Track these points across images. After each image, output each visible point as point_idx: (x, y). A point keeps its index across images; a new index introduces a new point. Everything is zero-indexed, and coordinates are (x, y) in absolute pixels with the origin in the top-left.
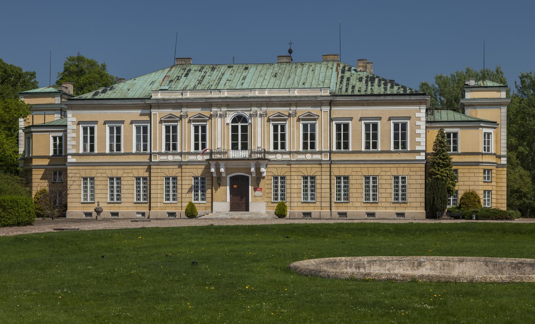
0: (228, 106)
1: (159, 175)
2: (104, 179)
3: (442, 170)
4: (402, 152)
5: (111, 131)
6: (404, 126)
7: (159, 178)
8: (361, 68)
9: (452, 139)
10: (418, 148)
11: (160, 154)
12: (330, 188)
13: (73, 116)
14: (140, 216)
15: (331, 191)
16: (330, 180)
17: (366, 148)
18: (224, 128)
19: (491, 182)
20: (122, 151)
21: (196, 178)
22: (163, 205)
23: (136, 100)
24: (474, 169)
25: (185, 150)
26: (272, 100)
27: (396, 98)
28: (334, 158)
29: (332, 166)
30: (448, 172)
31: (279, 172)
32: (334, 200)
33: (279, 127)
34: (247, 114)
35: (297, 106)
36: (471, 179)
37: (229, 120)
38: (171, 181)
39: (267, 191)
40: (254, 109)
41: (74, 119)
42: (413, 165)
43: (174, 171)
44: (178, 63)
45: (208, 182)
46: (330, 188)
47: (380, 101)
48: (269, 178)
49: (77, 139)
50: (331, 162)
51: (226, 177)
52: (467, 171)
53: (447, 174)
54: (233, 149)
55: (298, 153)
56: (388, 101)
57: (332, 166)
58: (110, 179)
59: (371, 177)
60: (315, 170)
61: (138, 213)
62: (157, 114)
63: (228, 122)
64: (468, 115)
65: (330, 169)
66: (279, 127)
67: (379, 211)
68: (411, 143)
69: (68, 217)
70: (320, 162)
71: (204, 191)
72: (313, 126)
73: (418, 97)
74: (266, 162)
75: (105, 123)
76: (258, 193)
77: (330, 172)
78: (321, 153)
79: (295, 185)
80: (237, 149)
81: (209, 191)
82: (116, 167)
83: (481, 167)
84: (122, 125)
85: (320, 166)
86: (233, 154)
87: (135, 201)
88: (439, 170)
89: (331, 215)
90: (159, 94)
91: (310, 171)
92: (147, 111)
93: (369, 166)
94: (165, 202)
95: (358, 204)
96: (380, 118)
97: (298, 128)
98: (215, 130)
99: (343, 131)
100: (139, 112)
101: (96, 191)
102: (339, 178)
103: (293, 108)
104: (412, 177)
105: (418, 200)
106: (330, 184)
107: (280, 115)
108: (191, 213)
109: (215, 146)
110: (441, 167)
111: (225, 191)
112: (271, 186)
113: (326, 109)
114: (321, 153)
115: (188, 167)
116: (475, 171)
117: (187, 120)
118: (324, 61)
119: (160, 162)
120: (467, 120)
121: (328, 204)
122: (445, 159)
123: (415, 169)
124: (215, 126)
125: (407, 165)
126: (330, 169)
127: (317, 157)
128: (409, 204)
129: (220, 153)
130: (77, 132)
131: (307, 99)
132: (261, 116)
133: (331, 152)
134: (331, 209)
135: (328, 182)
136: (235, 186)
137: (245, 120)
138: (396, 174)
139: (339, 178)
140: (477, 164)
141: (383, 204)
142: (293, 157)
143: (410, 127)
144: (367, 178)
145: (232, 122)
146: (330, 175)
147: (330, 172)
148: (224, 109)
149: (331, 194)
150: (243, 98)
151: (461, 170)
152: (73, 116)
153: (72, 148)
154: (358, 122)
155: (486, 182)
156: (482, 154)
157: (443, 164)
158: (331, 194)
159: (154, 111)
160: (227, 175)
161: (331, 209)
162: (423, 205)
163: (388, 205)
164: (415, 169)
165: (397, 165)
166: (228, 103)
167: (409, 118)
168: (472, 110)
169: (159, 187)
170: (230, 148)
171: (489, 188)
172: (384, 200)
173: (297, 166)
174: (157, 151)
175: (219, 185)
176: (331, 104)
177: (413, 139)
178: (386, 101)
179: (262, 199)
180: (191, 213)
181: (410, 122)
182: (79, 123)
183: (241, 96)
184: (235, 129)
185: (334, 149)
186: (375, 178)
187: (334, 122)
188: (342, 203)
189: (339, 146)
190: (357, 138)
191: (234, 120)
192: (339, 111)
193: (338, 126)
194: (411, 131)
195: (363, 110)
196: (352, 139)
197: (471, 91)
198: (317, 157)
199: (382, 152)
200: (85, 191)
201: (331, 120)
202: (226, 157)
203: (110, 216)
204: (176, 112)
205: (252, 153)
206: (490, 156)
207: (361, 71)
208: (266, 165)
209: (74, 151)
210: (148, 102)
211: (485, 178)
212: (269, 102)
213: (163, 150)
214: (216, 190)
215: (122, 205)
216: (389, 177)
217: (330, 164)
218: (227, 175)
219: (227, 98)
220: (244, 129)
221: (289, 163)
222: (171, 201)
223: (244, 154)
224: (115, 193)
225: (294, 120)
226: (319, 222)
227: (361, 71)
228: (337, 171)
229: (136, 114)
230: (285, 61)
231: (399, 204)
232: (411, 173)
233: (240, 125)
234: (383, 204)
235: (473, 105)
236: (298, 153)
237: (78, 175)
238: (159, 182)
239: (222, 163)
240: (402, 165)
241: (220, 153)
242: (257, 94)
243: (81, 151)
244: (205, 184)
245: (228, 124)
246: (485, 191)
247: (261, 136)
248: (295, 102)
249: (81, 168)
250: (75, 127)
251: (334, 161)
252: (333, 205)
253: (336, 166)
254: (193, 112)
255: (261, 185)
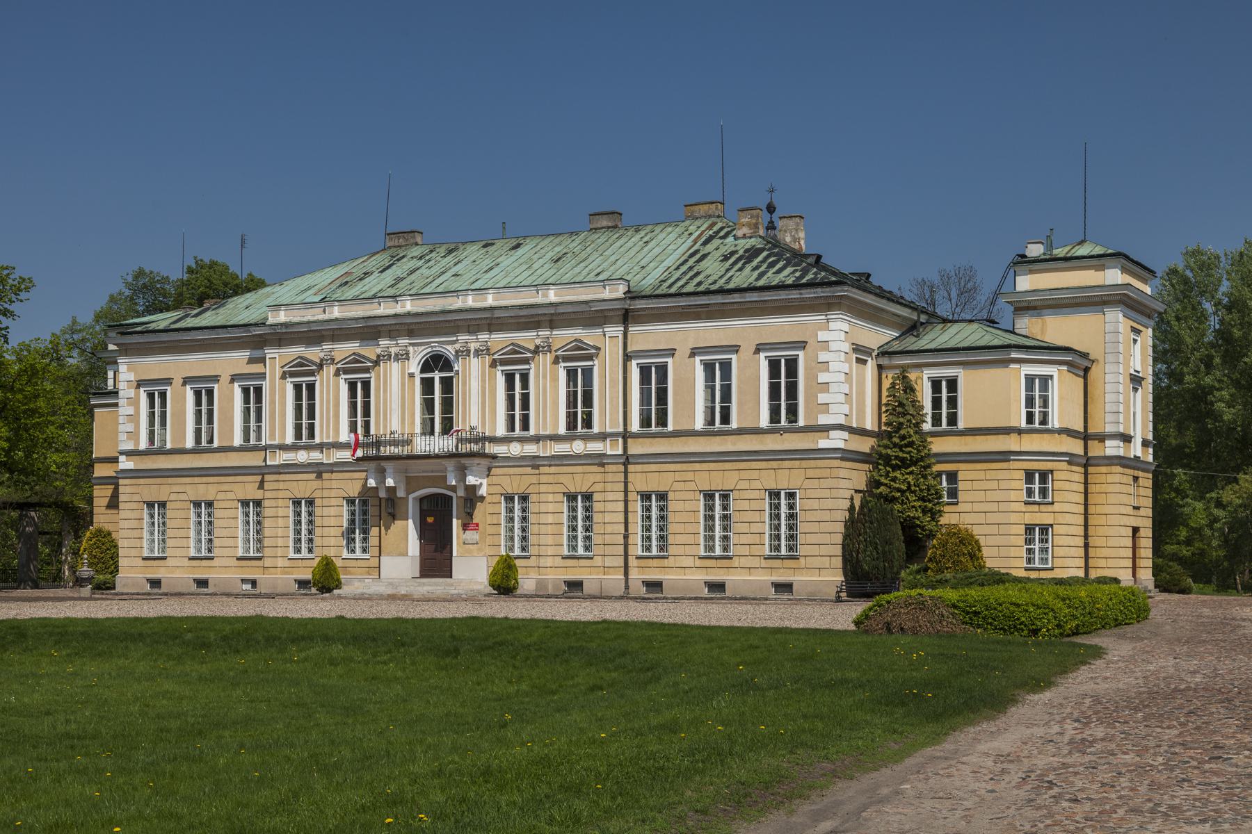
0: (411, 333)
1: (281, 494)
2: (690, 495)
3: (897, 474)
4: (786, 430)
5: (710, 376)
6: (792, 364)
7: (280, 503)
8: (745, 230)
9: (1037, 394)
10: (823, 420)
11: (283, 447)
12: (626, 523)
13: (129, 370)
14: (248, 587)
15: (626, 529)
16: (626, 502)
17: (642, 426)
18: (403, 385)
19: (1052, 503)
20: (734, 425)
21: (351, 502)
22: (287, 564)
23: (236, 330)
24: (996, 470)
25: (328, 437)
26: (498, 314)
27: (767, 296)
28: (636, 448)
29: (1091, 469)
30: (910, 478)
31: (515, 485)
32: (637, 549)
33: (517, 377)
34: (450, 351)
35: (552, 328)
36: (991, 496)
37: (414, 366)
38: (580, 504)
39: (491, 530)
40: (463, 338)
41: (132, 377)
42: (812, 463)
43: (304, 486)
44: (392, 244)
45: (372, 510)
46: (626, 523)
47: (735, 306)
48: (496, 498)
49: (134, 418)
50: (627, 460)
51: (406, 499)
52: (981, 475)
53: (909, 485)
54: (423, 434)
55: (555, 438)
56: (754, 305)
57: (1091, 469)
58: (705, 495)
59: (717, 495)
60: (592, 478)
61: (244, 581)
62: (278, 358)
63: (411, 371)
64: (1023, 332)
65: (626, 477)
66: (517, 377)
67: (734, 578)
68: (806, 407)
69: (119, 589)
70: (599, 460)
71: (365, 532)
72: (588, 372)
73: (819, 290)
74: (485, 462)
75: (693, 353)
76: (471, 535)
77: (626, 483)
78: (603, 437)
79: (551, 514)
80: (432, 433)
81: (374, 531)
82: (205, 479)
83: (1012, 465)
84: (216, 386)
85: (602, 469)
86: (422, 445)
87: (566, 553)
88: (887, 476)
89: (627, 587)
90: (282, 313)
91: (580, 480)
92: (257, 353)
93: (713, 466)
94: (292, 555)
95: (688, 562)
96: (735, 349)
97: (555, 379)
98: (385, 391)
99: (655, 380)
100: (246, 354)
101: (672, 528)
102: (646, 497)
103: (544, 333)
104: (810, 493)
105: (824, 550)
106: (626, 512)
107: (516, 349)
108: (326, 580)
109: (385, 427)
110: (895, 468)
111: (408, 534)
112: (499, 519)
113: (617, 330)
114: (603, 437)
115: (334, 475)
116: (1001, 475)
117: (332, 369)
118: (687, 218)
119: (336, 464)
120: (1000, 343)
121: (621, 562)
122: (906, 446)
123: (818, 473)
124: (385, 382)
125: (797, 463)
126: (626, 477)
127: (595, 447)
128: (802, 560)
129: (395, 443)
130: (135, 402)
131: (570, 309)
132: (478, 353)
133: (626, 435)
134: (626, 574)
135: (621, 506)
136: (430, 520)
137: (446, 364)
138: (772, 486)
139: (646, 497)
140: (1004, 456)
141: (744, 562)
142: (545, 447)
143: (806, 369)
144: (774, 494)
145: (422, 371)
146: (626, 492)
147: (626, 483)
148: (403, 341)
149: (626, 537)
150: (443, 312)
151: (966, 473)
152: (129, 370)
153: (129, 438)
154: (688, 360)
155: (1035, 503)
156: (1020, 431)
157: (903, 460)
158: (626, 537)
159: (270, 353)
160: (409, 492)
161: (626, 574)
162: (838, 562)
163: (756, 562)
164: (818, 473)
165: (774, 464)
166: (412, 327)
167: (802, 345)
168: (1034, 319)
169: (281, 522)
170: (418, 430)
171: (1046, 519)
172: (745, 550)
173: (553, 470)
174: (276, 442)
175: (394, 517)
176: (627, 317)
177: (811, 397)
178: (749, 306)
179: (480, 550)
180: (326, 580)
181: (738, 360)
182: (140, 384)
183: (437, 309)
184: (428, 385)
185: (635, 426)
186: (725, 497)
187: (634, 362)
188: (716, 558)
189: (646, 422)
190: (690, 401)
191: (426, 367)
192: (646, 336)
193: (645, 371)
194: (806, 378)
195: (698, 330)
196: (675, 401)
197: (1031, 272)
198: (595, 447)
199: (740, 432)
200: (199, 533)
201: (627, 358)
202: (406, 451)
203: (194, 588)
204: (313, 353)
205: (460, 440)
206: (1045, 435)
207: (744, 236)
208: (489, 469)
209: (129, 446)
210: (258, 331)
211: (1030, 492)
212: (490, 321)
213: (562, 430)
214: (387, 528)
215: (215, 563)
216: (755, 494)
217: (625, 464)
218: (409, 492)
219: (408, 314)
220: (447, 385)
221: (534, 462)
222: (359, 553)
223: (440, 444)
224: (517, 532)
225: (545, 360)
226: (247, 609)
227: (744, 236)
228: (642, 479)
229: (238, 360)
230: (605, 223)
231: (779, 561)
232: (808, 484)
233: (437, 376)
234: (744, 562)
235: (1035, 308)
236: (555, 438)
237: (136, 498)
238: (281, 512)
239: (389, 466)
240: (787, 464)
241: (395, 443)
242: (470, 301)
243: (143, 445)
244: (372, 512)
245: (412, 375)
246: (1029, 529)
247: (481, 400)
248: (547, 318)
249: (142, 481)
250: (132, 393)
251: (632, 455)
252: (632, 562)
253: (639, 468)
254: (343, 350)
255: (478, 517)
